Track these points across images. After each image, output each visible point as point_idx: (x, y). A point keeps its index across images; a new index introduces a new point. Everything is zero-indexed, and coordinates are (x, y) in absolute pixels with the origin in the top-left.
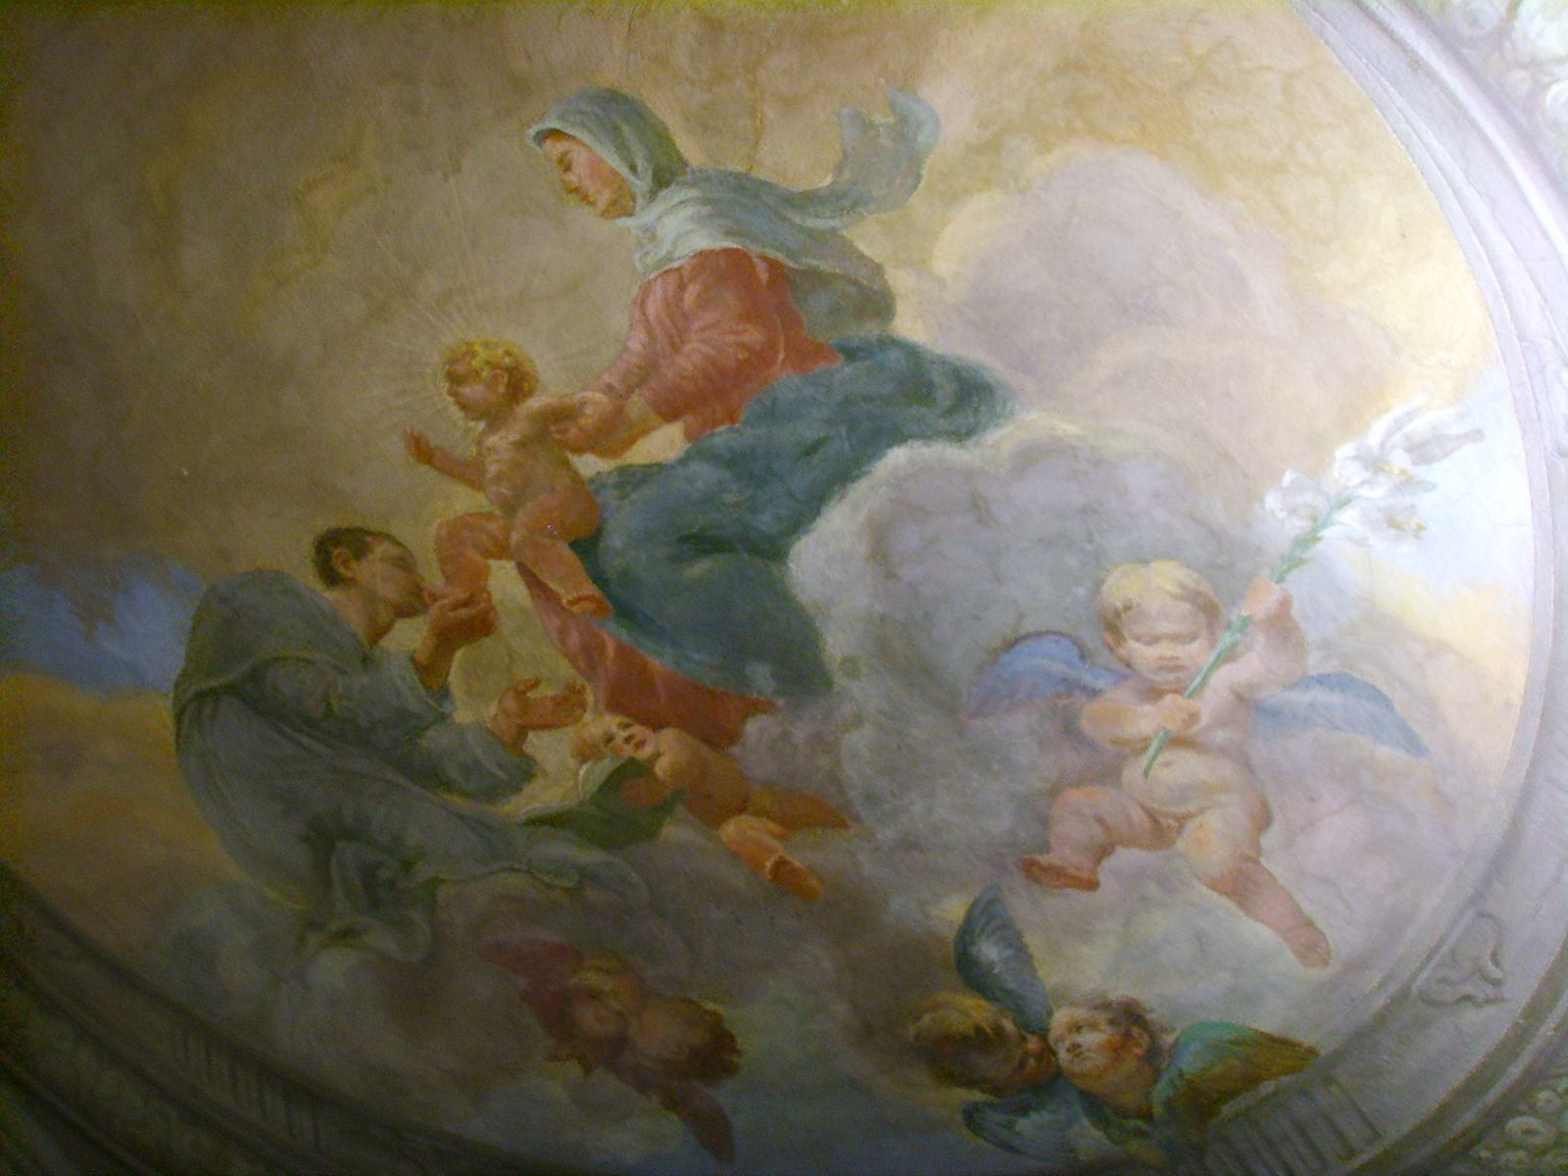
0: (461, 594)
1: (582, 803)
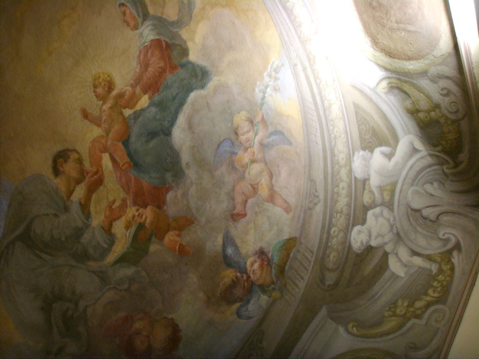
0: (94, 169)
1: (128, 248)
